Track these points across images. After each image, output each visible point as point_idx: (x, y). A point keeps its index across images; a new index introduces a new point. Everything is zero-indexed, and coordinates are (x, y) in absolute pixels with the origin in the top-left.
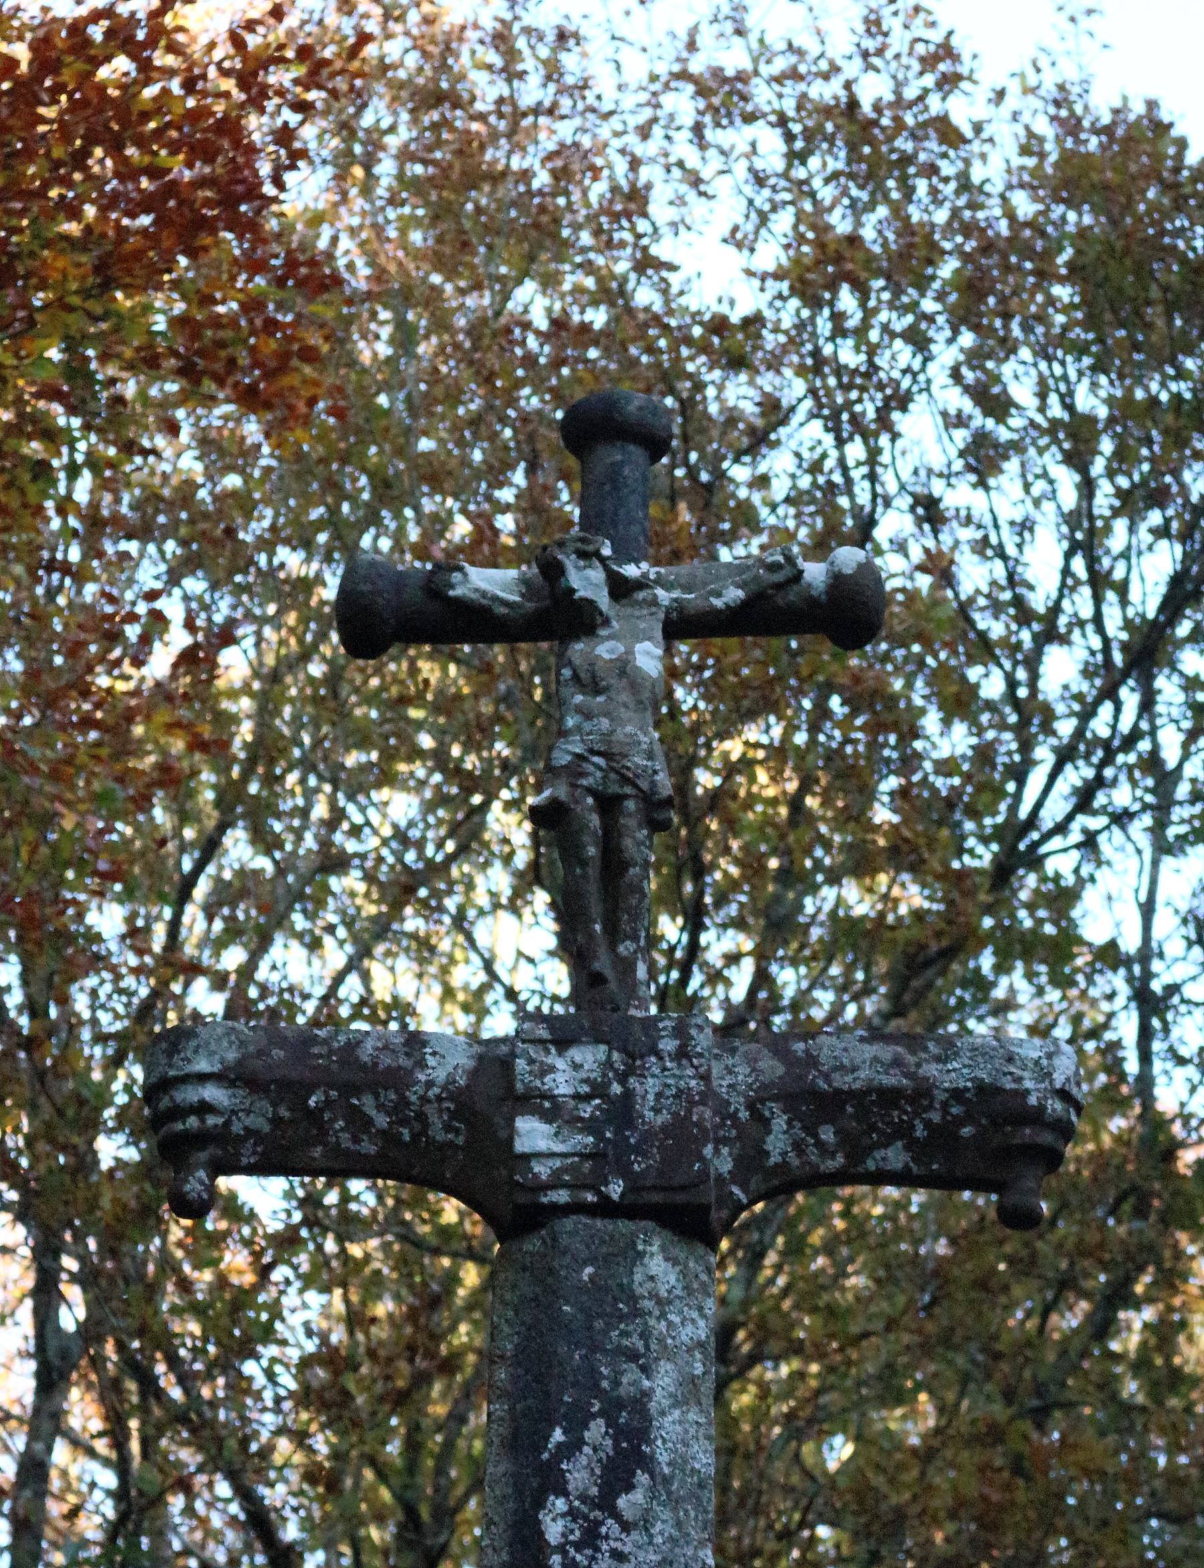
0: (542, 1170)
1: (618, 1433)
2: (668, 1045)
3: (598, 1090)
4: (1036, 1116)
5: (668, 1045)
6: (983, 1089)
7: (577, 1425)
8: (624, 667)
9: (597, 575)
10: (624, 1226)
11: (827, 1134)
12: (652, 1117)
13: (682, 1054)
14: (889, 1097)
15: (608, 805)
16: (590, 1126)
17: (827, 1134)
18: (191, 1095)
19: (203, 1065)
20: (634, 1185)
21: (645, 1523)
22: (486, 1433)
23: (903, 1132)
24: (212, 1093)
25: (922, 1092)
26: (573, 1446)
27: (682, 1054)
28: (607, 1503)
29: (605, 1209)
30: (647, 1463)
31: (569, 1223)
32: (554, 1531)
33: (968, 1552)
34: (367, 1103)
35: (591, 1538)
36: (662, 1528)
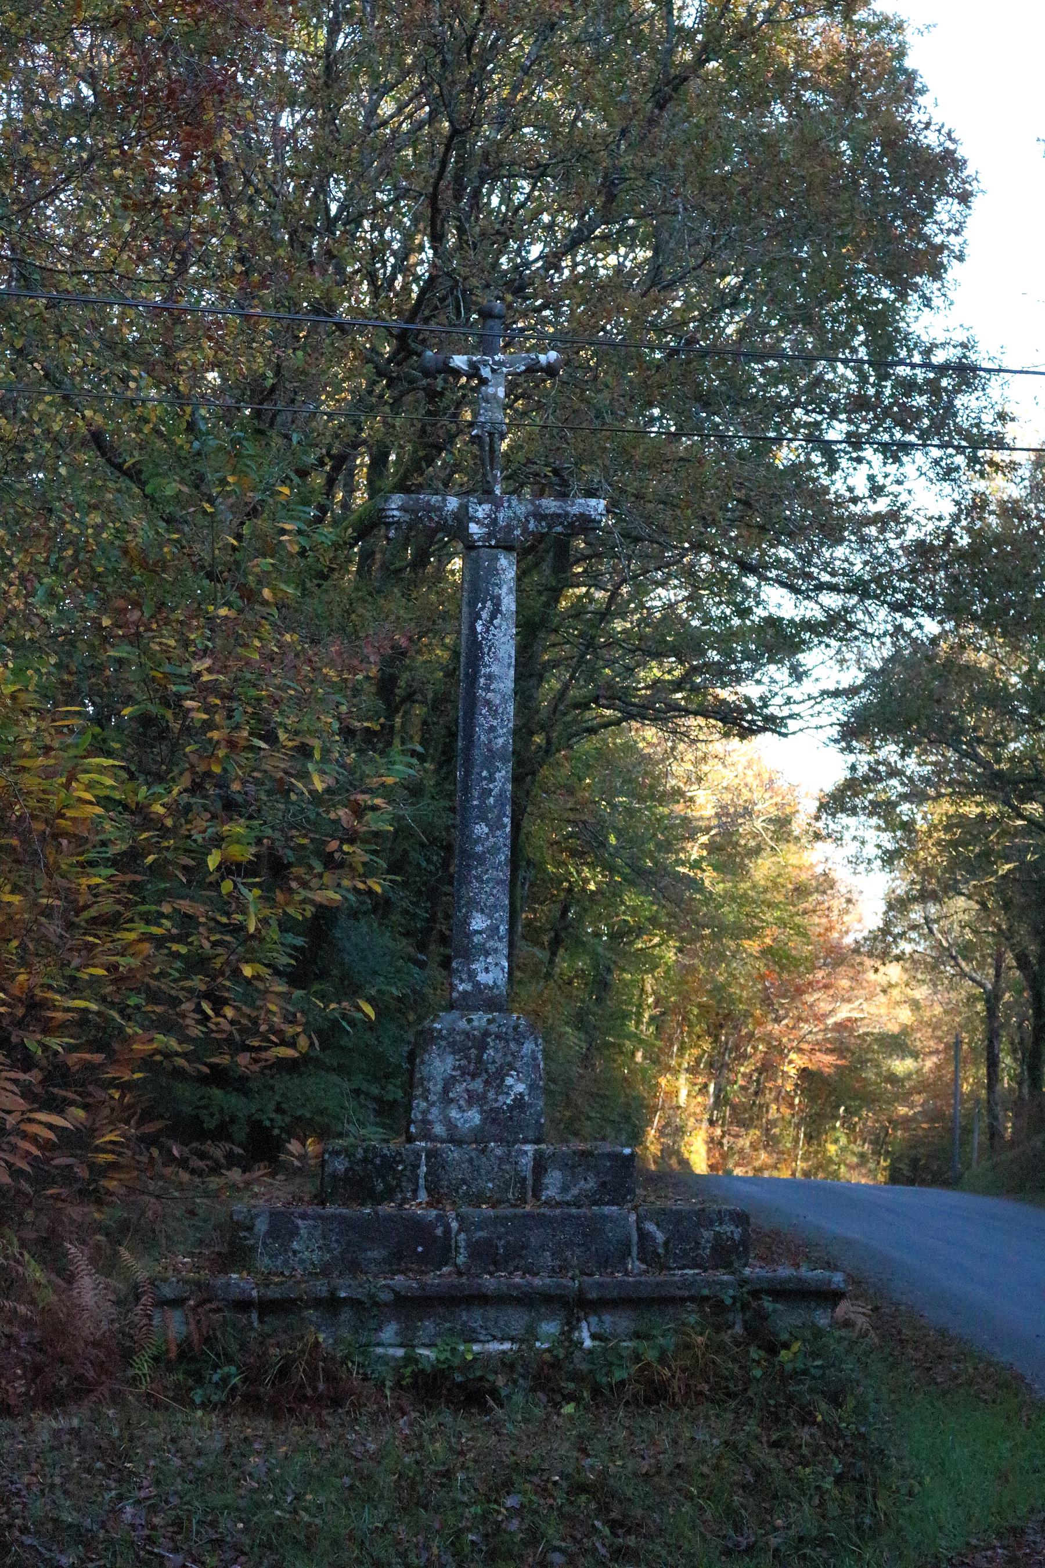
0: (476, 537)
1: (494, 605)
2: (506, 505)
3: (489, 516)
4: (594, 521)
5: (506, 505)
6: (582, 514)
7: (484, 603)
8: (495, 395)
9: (488, 369)
10: (495, 551)
11: (543, 524)
12: (502, 523)
13: (509, 507)
14: (559, 516)
15: (491, 434)
16: (487, 526)
17: (543, 524)
18: (391, 513)
19: (393, 506)
20: (498, 541)
21: (500, 627)
22: (1006, 1128)
23: (561, 523)
24: (395, 513)
25: (567, 514)
26: (482, 609)
27: (509, 507)
28: (491, 622)
29: (490, 547)
30: (500, 612)
31: (482, 550)
32: (479, 629)
33: (262, 1226)
34: (433, 515)
35: (488, 631)
36: (503, 628)
